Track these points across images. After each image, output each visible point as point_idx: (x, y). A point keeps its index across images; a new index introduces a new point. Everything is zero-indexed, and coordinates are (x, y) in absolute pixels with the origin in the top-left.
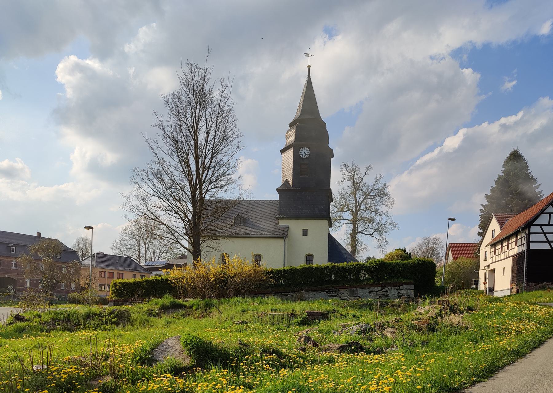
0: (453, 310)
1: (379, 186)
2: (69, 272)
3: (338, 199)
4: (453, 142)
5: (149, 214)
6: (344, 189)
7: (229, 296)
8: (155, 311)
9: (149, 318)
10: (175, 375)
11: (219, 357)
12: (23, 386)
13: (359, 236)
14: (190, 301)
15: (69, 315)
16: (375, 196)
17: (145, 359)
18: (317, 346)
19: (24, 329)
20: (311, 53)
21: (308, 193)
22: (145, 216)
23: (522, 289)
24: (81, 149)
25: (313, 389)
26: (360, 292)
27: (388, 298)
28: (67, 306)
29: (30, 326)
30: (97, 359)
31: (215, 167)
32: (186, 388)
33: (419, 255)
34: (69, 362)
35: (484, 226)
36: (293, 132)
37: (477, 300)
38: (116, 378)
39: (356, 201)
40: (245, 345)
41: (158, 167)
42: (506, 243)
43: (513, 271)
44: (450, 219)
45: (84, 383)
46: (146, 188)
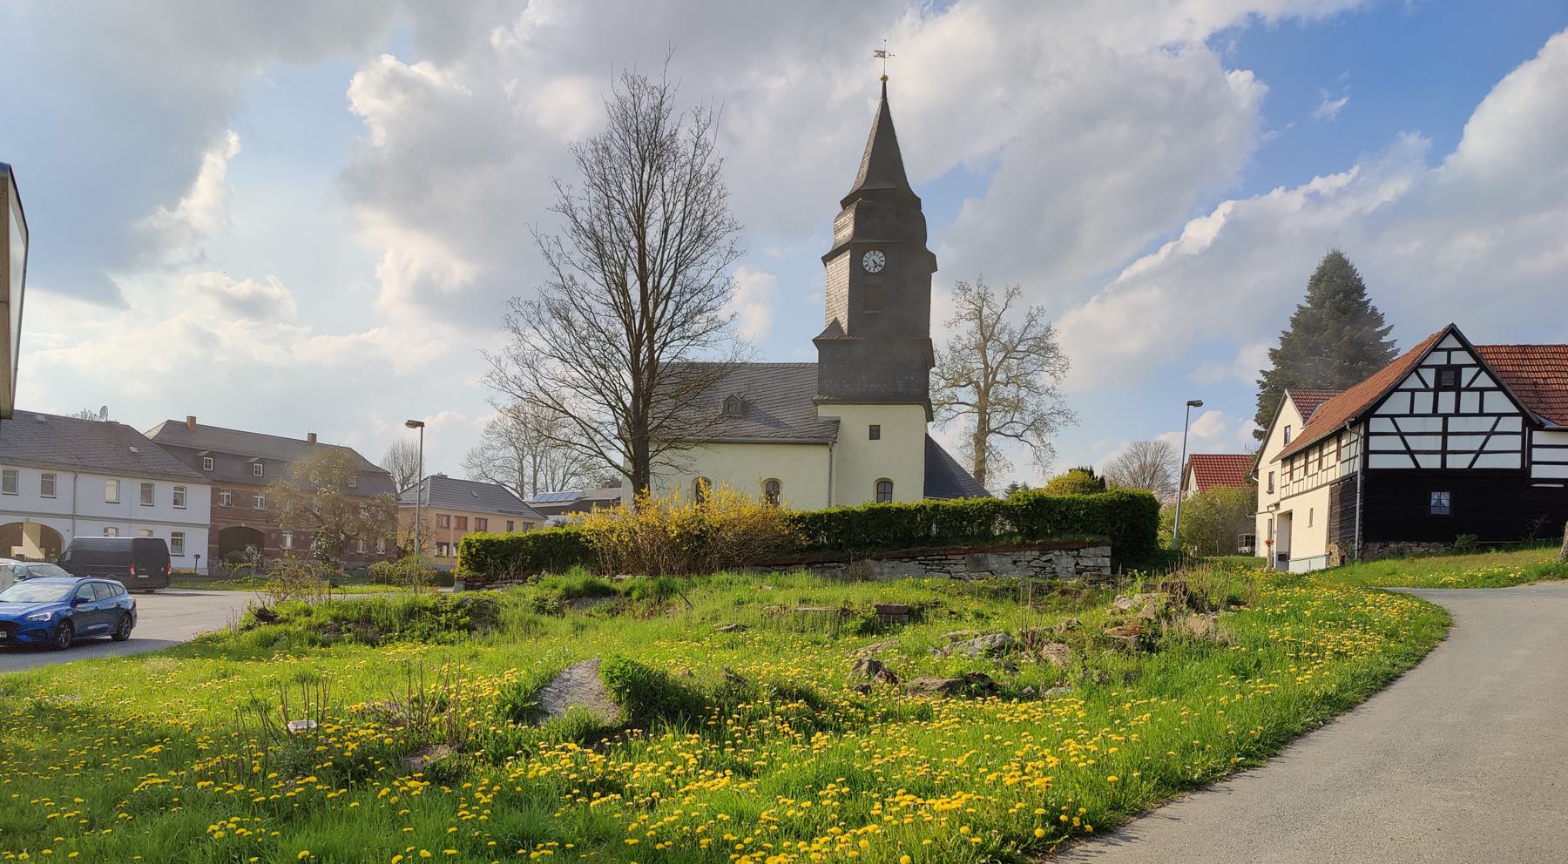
0: (1196, 604)
1: (1036, 331)
2: (373, 516)
3: (947, 360)
4: (1202, 232)
5: (541, 395)
6: (959, 338)
7: (710, 571)
8: (552, 602)
9: (538, 616)
10: (587, 744)
11: (682, 706)
12: (266, 765)
13: (992, 439)
14: (627, 580)
15: (369, 610)
16: (1029, 352)
17: (523, 710)
18: (895, 680)
19: (276, 640)
20: (888, 50)
21: (881, 345)
22: (533, 400)
23: (1351, 557)
24: (398, 253)
25: (881, 779)
26: (993, 561)
27: (1055, 575)
28: (365, 588)
29: (287, 633)
30: (422, 709)
31: (682, 294)
32: (609, 773)
33: (1126, 484)
34: (362, 715)
35: (1267, 418)
36: (849, 218)
37: (1250, 581)
38: (460, 751)
39: (986, 363)
40: (738, 680)
41: (559, 296)
42: (1317, 456)
43: (1331, 516)
44: (1190, 404)
45: (392, 761)
46: (538, 340)
